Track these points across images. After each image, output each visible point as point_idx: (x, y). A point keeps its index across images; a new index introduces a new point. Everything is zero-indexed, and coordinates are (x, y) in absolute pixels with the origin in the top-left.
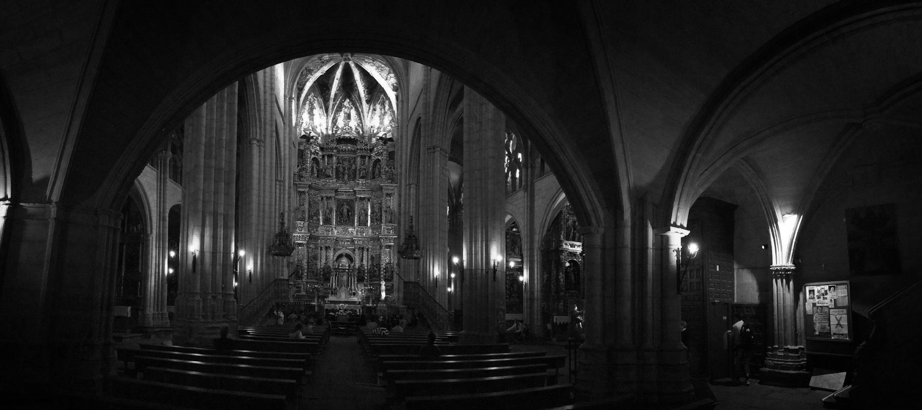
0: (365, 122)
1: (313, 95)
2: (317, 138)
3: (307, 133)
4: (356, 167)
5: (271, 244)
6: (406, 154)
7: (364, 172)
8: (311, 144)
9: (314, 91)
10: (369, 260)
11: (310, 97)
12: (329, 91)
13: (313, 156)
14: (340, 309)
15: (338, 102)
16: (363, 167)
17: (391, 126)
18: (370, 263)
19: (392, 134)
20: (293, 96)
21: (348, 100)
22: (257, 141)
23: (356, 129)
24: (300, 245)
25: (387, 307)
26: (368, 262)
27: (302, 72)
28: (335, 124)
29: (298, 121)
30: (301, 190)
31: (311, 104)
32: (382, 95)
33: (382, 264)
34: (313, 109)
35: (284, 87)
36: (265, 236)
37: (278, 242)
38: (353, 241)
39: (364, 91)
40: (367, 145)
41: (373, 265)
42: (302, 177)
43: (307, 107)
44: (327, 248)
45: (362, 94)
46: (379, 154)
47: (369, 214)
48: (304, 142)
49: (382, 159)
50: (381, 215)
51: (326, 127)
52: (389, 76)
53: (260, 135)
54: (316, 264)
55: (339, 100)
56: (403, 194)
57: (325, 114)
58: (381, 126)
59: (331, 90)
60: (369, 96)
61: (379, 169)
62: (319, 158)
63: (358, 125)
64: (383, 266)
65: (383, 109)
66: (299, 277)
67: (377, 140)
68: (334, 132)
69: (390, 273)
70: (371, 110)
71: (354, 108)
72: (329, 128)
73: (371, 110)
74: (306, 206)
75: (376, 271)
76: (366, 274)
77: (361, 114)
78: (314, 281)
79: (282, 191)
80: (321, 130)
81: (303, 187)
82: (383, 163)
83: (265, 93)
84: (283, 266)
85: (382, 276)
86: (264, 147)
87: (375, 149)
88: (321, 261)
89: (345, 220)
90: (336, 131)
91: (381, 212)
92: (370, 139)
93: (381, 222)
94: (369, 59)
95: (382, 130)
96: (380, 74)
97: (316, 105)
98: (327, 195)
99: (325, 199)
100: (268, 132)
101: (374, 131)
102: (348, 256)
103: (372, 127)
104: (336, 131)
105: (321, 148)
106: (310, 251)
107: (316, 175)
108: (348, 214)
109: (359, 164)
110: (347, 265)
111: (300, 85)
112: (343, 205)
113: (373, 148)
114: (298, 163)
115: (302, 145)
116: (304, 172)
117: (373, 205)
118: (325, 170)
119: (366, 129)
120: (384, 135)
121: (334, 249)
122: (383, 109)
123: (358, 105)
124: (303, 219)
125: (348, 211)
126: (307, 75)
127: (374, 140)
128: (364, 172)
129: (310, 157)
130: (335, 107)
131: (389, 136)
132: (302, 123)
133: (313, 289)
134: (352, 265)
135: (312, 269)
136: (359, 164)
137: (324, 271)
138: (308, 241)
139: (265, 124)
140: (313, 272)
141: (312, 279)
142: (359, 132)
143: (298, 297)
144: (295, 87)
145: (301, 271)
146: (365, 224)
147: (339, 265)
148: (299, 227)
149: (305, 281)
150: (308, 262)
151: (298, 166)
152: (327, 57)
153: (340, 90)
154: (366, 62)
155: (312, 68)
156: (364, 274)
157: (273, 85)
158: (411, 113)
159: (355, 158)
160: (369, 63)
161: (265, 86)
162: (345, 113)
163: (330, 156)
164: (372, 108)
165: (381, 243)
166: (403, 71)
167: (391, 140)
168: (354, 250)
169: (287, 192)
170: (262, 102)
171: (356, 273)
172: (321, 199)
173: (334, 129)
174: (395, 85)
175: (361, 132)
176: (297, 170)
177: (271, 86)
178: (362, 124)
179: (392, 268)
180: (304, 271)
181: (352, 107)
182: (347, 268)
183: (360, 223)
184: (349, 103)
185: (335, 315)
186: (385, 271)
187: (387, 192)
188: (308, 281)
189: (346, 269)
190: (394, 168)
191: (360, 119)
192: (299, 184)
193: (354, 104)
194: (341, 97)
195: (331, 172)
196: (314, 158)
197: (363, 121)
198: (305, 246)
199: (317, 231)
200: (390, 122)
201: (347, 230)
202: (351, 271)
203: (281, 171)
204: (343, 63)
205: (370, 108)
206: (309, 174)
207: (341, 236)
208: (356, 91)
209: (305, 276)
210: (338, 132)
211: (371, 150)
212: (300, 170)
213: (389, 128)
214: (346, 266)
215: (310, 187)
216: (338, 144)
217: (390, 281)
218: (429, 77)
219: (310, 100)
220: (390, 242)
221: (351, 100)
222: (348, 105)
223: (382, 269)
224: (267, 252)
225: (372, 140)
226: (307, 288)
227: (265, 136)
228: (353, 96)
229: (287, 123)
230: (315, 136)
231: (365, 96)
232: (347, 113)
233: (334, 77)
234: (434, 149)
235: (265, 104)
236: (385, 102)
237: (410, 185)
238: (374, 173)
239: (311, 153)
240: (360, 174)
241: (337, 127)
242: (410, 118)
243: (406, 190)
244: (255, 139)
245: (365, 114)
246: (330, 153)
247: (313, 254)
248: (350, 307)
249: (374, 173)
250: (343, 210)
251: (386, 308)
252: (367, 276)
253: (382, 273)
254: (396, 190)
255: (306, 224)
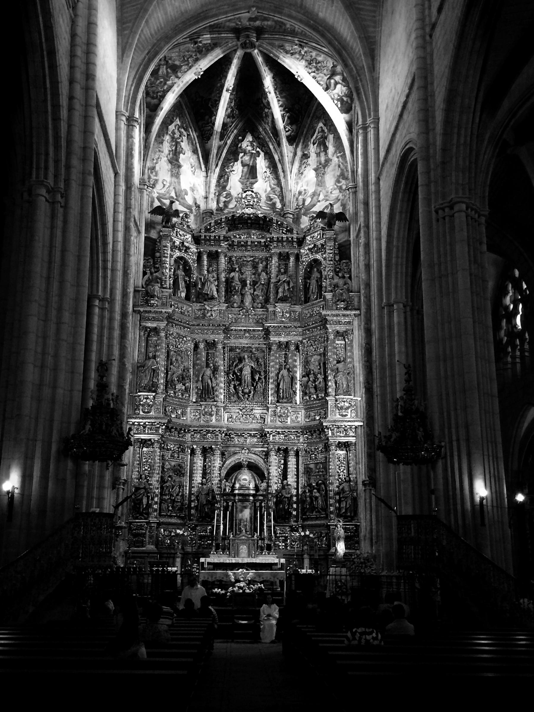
0: (287, 181)
1: (179, 123)
2: (187, 216)
3: (164, 204)
4: (269, 279)
5: (72, 433)
6: (379, 239)
7: (287, 288)
8: (173, 227)
9: (181, 116)
10: (300, 475)
11: (172, 127)
12: (211, 117)
13: (177, 254)
14: (238, 581)
15: (229, 142)
16: (284, 278)
17: (340, 188)
18: (302, 481)
19: (344, 206)
20: (137, 115)
21: (249, 138)
22: (48, 192)
23: (269, 199)
24: (144, 443)
25: (350, 575)
26: (298, 478)
27: (155, 73)
28: (224, 188)
29: (146, 177)
30: (149, 325)
31: (175, 142)
32: (321, 125)
33: (332, 484)
34: (179, 153)
35: (116, 92)
36: (57, 416)
37: (88, 427)
38: (263, 435)
39: (283, 117)
40: (291, 231)
41: (310, 485)
42: (153, 296)
43: (166, 147)
44: (206, 452)
45: (280, 124)
46: (315, 249)
47: (298, 375)
48: (158, 224)
49: (325, 259)
50: (325, 379)
51: (204, 194)
52: (332, 81)
53: (56, 176)
54: (181, 486)
55: (232, 138)
56: (374, 326)
57: (203, 166)
58: (319, 189)
59: (216, 115)
60: (294, 127)
61: (319, 280)
62: (191, 258)
63: (272, 189)
64: (334, 487)
65: (322, 154)
66: (141, 514)
67: (313, 218)
68: (221, 205)
69: (349, 502)
70: (298, 158)
71: (262, 154)
72: (212, 196)
73: (298, 158)
74: (162, 360)
75: (316, 498)
76: (295, 506)
77: (279, 166)
78: (173, 520)
79: (106, 321)
80: (195, 199)
81: (155, 319)
82: (327, 270)
83: (72, 81)
84: (101, 487)
85: (332, 509)
86: (66, 207)
87: (308, 238)
88: (191, 479)
89: (247, 391)
90: (226, 204)
91: (325, 372)
92: (297, 220)
93: (327, 394)
94: (293, 42)
95: (321, 197)
96: (314, 77)
97: (185, 145)
98: (206, 337)
99: (202, 346)
100: (75, 175)
101: (304, 201)
102: (253, 468)
103: (300, 193)
104: (225, 202)
105: (193, 237)
106: (168, 455)
107: (183, 295)
108: (253, 379)
109: (274, 270)
110: (252, 486)
111: (153, 98)
112: (241, 360)
113: (304, 238)
114: (144, 266)
115: (154, 228)
116: (157, 287)
117: (306, 358)
118: (203, 284)
119: (289, 197)
120: (327, 207)
121: (223, 454)
122: (322, 154)
123: (271, 147)
124: (152, 388)
125: (253, 372)
126: (167, 77)
127: (305, 222)
128: (287, 288)
129: (171, 256)
130: (225, 151)
131: (337, 209)
132: (157, 181)
133: (171, 538)
134: (264, 485)
135: (172, 495)
136: (274, 270)
137: (198, 500)
138: (163, 436)
139: (69, 154)
140: (173, 501)
141: (171, 517)
142: (274, 204)
143: (136, 555)
144: (140, 96)
145: (145, 501)
146: (290, 399)
147: (233, 488)
148: (143, 405)
149: (155, 520)
150: (163, 481)
151: (145, 273)
152: (207, 39)
153: (233, 117)
154: (287, 52)
155: (177, 63)
156: (290, 504)
157: (91, 66)
158: (386, 147)
159: (267, 259)
160: (292, 54)
161: (72, 67)
162: (243, 165)
163: (214, 257)
164: (299, 153)
165: (328, 439)
166: (364, 61)
167: (341, 217)
168: (267, 455)
169: (117, 325)
170: (64, 101)
171: (271, 504)
172: (193, 346)
173: (222, 199)
174: (345, 99)
175: (279, 205)
176: (140, 282)
177: (88, 69)
178: (281, 188)
179: (353, 490)
180: (153, 499)
181: (258, 152)
182: (252, 492)
183: (278, 396)
184: (251, 143)
185: (226, 593)
186: (337, 497)
187: (338, 328)
188: (162, 520)
189: (249, 495)
190: (350, 278)
191: (277, 178)
192: (146, 312)
193: (262, 145)
194: (235, 131)
195: (214, 289)
196: (181, 258)
197: (283, 180)
198: (156, 445)
199: (184, 414)
200: (338, 181)
201: (249, 413)
202: (261, 498)
203: (105, 277)
204: (239, 53)
205: (295, 154)
206: (169, 291)
207: (237, 425)
208: (267, 116)
209: (156, 510)
210: (231, 206)
211: (301, 242)
212: (149, 283)
213: (336, 193)
214: (248, 489)
215: (169, 318)
216: (229, 230)
217: (352, 518)
218: (428, 49)
219: (173, 133)
220: (347, 436)
221: (257, 137)
222: (249, 148)
223: (332, 493)
224: (58, 452)
225: (302, 220)
226: (158, 537)
227: (67, 181)
228: (261, 129)
229: (122, 171)
230: (182, 212)
231: (285, 128)
232: (248, 165)
233: (222, 86)
234: (451, 208)
235: (71, 109)
236: (326, 138)
237: (390, 306)
238: (306, 289)
239: (174, 247)
240: (277, 293)
241: (229, 195)
242: (386, 158)
243: (381, 317)
244: (41, 184)
245: (287, 165)
246: (214, 249)
247: (173, 464)
248: (259, 575)
249: (306, 289)
250: (241, 370)
251: (348, 578)
252: (295, 509)
253: (332, 501)
254: (356, 323)
255: (160, 399)
